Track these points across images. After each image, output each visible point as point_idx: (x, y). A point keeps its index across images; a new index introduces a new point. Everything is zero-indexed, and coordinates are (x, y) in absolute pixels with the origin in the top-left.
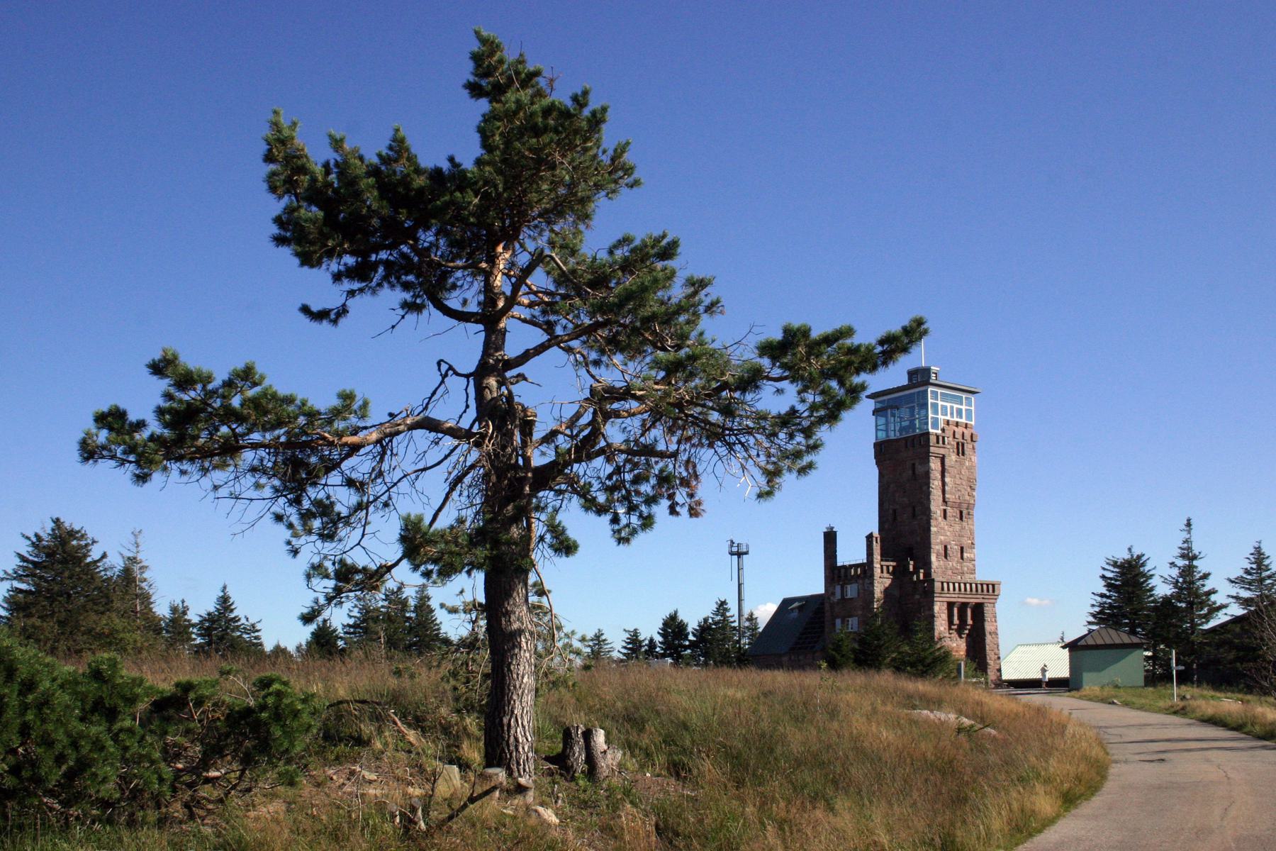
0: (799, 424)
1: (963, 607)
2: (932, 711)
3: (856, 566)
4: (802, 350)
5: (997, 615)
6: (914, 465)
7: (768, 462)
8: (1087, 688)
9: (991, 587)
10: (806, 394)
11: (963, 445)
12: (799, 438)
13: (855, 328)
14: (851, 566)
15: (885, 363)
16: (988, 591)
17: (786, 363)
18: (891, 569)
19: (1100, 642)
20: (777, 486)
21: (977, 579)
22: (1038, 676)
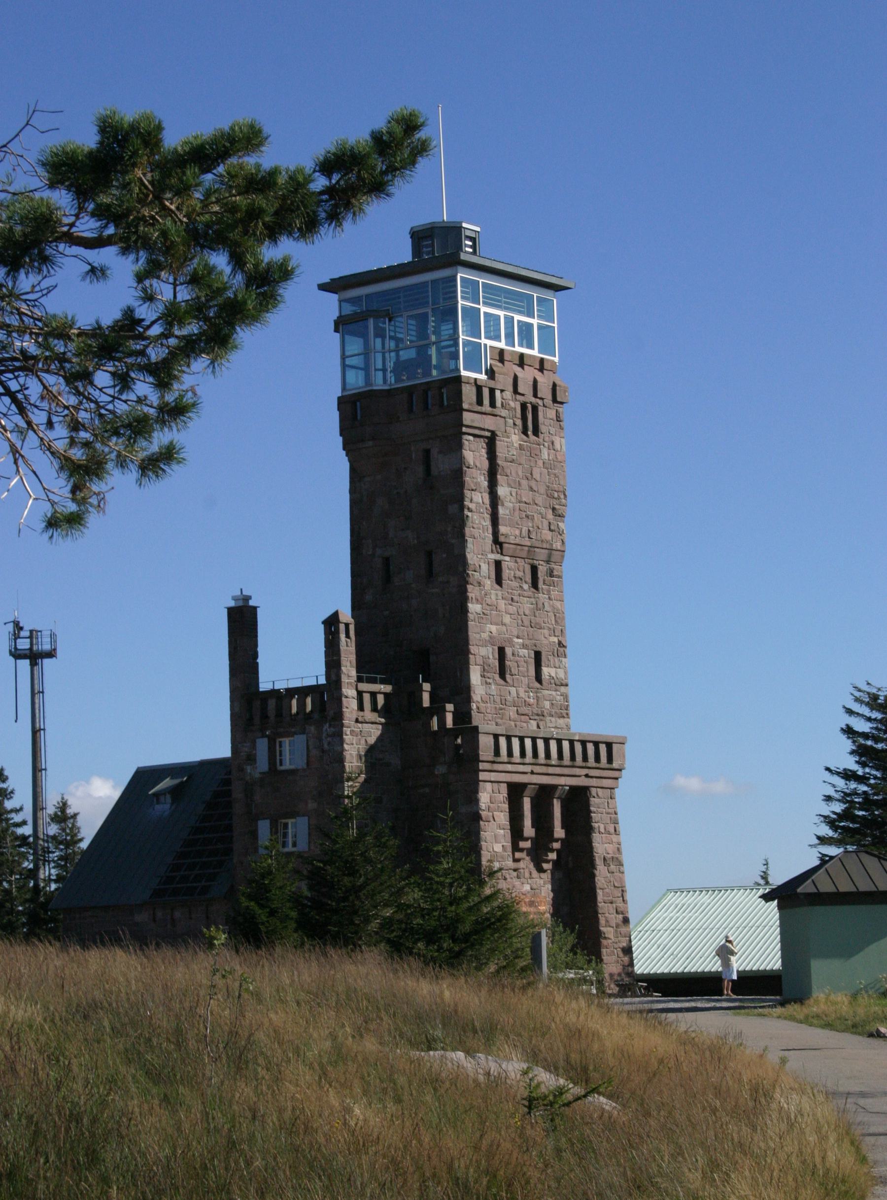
0: (142, 353)
1: (544, 794)
2: (469, 1052)
3: (302, 692)
4: (143, 174)
5: (620, 817)
6: (427, 452)
7: (72, 442)
8: (822, 996)
9: (603, 749)
10: (155, 282)
11: (535, 409)
12: (143, 387)
13: (266, 130)
14: (291, 692)
15: (334, 217)
16: (597, 759)
17: (108, 206)
18: (381, 700)
19: (845, 886)
20: (94, 501)
21: (573, 730)
22: (712, 965)
